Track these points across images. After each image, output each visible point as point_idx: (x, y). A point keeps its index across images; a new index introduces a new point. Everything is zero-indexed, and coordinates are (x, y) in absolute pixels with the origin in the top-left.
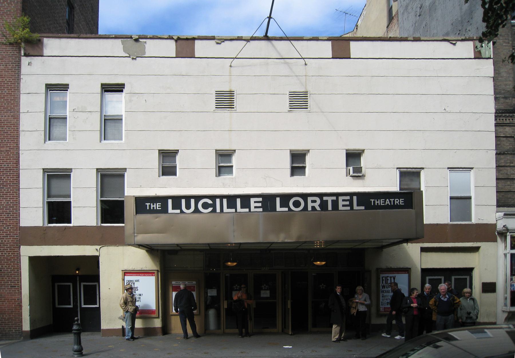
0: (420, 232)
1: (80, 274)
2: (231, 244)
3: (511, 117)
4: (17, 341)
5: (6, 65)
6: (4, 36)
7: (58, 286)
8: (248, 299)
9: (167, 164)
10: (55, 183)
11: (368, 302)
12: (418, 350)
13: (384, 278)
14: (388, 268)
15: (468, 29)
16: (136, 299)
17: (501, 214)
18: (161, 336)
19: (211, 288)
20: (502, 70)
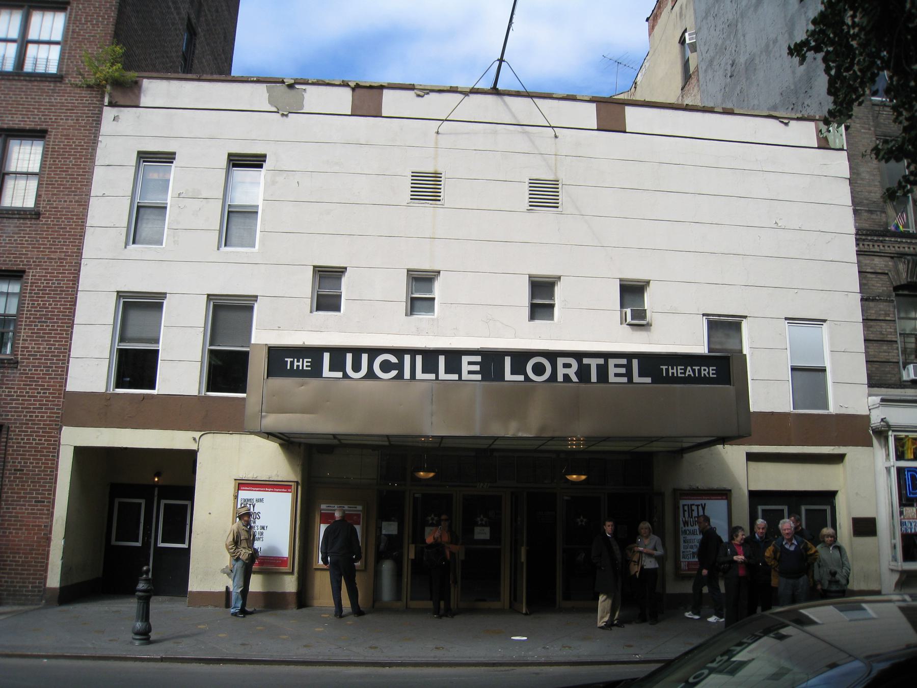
0: (743, 426)
1: (160, 483)
2: (428, 437)
4: (32, 607)
6: (80, 74)
7: (120, 503)
8: (451, 543)
10: (135, 317)
11: (660, 552)
12: (749, 644)
13: (686, 508)
14: (694, 490)
15: (806, 103)
16: (254, 536)
17: (877, 399)
18: (295, 611)
19: (388, 520)
20: (862, 169)
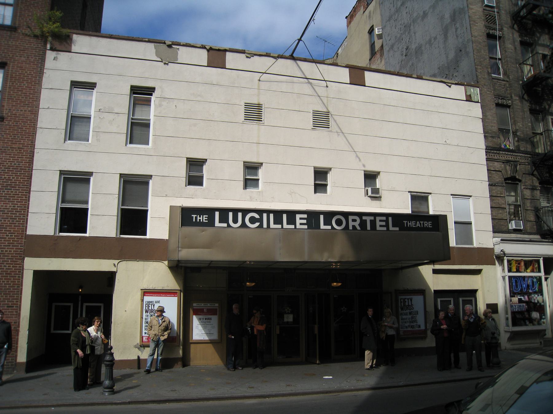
3: (498, 154)
5: (28, 57)
6: (29, 27)
9: (192, 174)
10: (71, 187)
11: (396, 326)
13: (402, 300)
15: (455, 75)
17: (499, 239)
20: (488, 114)
